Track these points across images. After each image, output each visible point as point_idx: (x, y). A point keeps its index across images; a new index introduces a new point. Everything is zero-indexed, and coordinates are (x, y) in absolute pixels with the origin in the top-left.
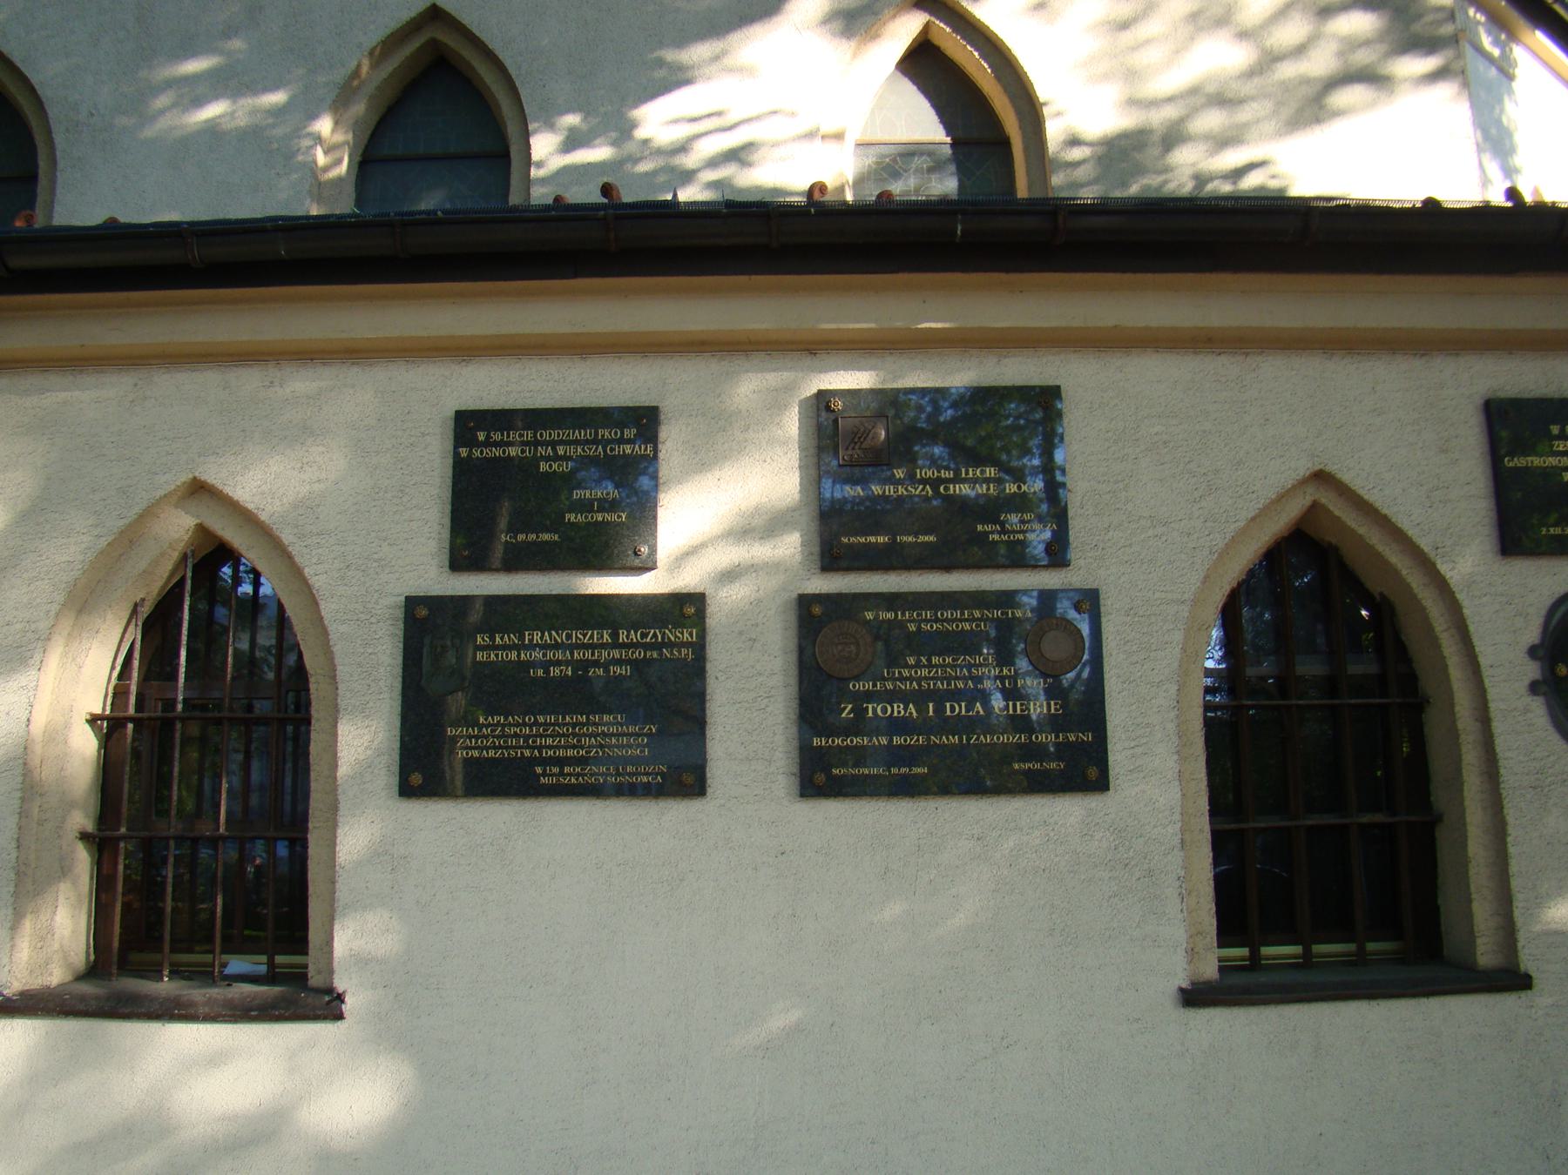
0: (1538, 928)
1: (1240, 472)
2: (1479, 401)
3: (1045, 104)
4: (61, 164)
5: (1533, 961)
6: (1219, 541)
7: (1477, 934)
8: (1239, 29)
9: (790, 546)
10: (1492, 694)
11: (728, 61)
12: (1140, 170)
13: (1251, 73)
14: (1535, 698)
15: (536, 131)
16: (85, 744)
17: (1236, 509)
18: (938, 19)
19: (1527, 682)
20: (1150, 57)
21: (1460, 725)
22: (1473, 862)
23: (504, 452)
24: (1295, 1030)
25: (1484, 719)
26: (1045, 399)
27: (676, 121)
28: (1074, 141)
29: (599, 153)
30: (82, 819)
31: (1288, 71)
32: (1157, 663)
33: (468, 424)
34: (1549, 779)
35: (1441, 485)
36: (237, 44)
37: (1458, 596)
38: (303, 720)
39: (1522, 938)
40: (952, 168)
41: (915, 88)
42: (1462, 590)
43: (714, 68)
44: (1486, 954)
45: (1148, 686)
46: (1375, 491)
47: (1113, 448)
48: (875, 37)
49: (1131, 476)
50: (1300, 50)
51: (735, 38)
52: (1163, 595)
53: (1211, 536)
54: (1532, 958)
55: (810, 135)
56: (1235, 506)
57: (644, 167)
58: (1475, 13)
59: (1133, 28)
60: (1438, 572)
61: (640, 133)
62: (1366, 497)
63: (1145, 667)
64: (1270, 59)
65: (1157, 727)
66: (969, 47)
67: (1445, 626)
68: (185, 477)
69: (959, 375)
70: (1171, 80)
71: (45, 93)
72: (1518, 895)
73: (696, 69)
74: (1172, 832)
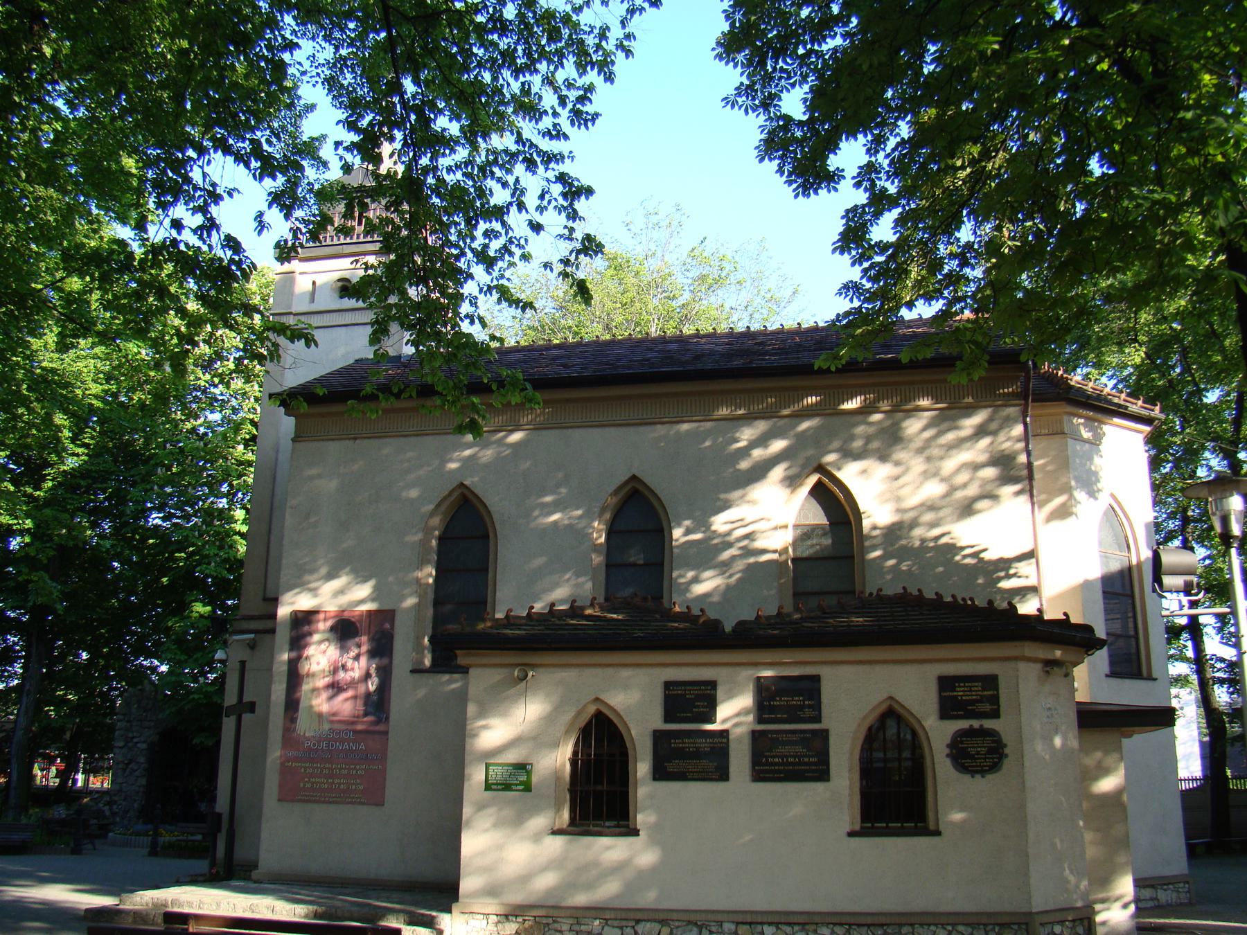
4: (499, 537)
9: (750, 718)
12: (900, 538)
15: (674, 527)
16: (568, 767)
25: (933, 764)
26: (816, 679)
27: (726, 523)
28: (875, 528)
29: (698, 536)
30: (568, 786)
31: (959, 495)
33: (668, 685)
36: (563, 490)
38: (626, 763)
40: (830, 535)
44: (932, 827)
50: (965, 486)
51: (748, 488)
55: (776, 528)
57: (715, 541)
61: (713, 528)
64: (953, 489)
68: (594, 697)
69: (795, 672)
70: (913, 501)
71: (492, 509)
74: (847, 792)
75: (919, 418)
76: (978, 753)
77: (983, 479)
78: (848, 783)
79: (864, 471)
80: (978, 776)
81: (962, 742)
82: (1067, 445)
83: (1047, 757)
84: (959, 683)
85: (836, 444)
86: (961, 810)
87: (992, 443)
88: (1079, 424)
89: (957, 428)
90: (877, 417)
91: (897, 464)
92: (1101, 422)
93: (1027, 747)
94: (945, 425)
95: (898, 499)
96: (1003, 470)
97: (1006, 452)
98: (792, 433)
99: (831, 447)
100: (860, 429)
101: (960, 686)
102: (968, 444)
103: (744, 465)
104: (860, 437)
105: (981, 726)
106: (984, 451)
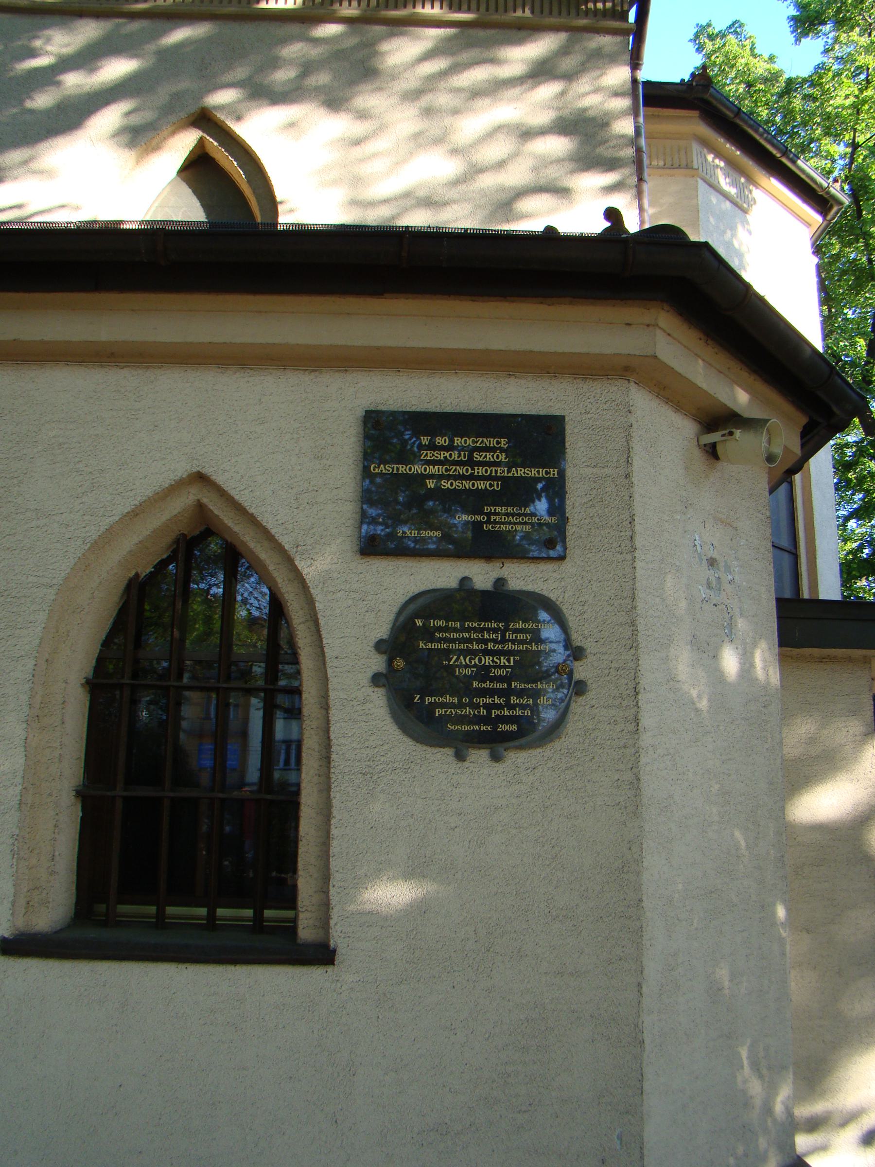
0: (352, 908)
1: (123, 472)
2: (360, 413)
3: (281, 203)
5: (344, 938)
6: (93, 533)
7: (300, 909)
8: (451, 146)
10: (333, 683)
11: (35, 165)
13: (456, 182)
14: (376, 689)
17: (114, 505)
18: (208, 135)
19: (370, 674)
20: (377, 166)
21: (261, 713)
22: (304, 840)
23: (473, 485)
24: (104, 985)
32: (20, 640)
34: (380, 767)
35: (311, 489)
37: (312, 591)
39: (335, 914)
41: (190, 190)
42: (317, 586)
43: (21, 170)
44: (306, 931)
45: (10, 660)
46: (246, 492)
47: (14, 449)
48: (157, 148)
49: (26, 474)
50: (501, 165)
51: (43, 146)
52: (35, 579)
53: (87, 529)
54: (343, 935)
56: (114, 502)
58: (714, 159)
59: (363, 144)
60: (296, 567)
62: (236, 497)
63: (9, 643)
65: (11, 698)
66: (230, 157)
67: (302, 620)
72: (336, 874)
73: (7, 170)
75: (418, 38)
76: (484, 673)
77: (537, 157)
78: (20, 761)
79: (292, 125)
80: (479, 756)
81: (429, 634)
82: (696, 190)
83: (704, 704)
84: (433, 434)
85: (241, 72)
86: (410, 874)
87: (563, 93)
88: (717, 166)
89: (494, 61)
90: (331, 29)
91: (362, 115)
92: (751, 180)
93: (647, 662)
94: (465, 56)
95: (357, 181)
96: (582, 143)
97: (591, 113)
98: (151, 47)
99: (229, 77)
100: (293, 50)
101: (432, 447)
102: (516, 91)
103: (42, 101)
104: (290, 62)
105: (500, 582)
106: (546, 106)
